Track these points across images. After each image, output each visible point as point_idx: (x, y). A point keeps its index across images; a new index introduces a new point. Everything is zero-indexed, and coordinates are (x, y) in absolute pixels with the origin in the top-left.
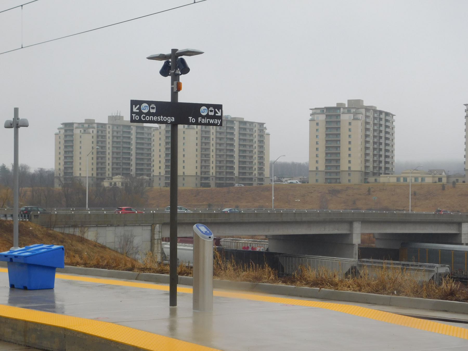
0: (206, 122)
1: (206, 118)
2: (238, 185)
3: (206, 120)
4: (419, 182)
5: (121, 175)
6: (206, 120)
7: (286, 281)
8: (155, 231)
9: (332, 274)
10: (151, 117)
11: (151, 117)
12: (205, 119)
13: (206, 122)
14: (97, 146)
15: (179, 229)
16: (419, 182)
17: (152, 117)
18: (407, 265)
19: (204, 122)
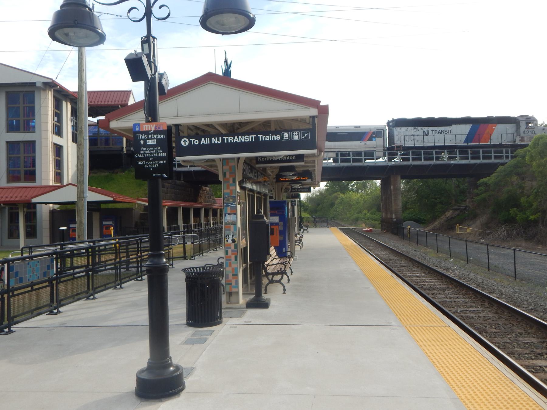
0: (270, 139)
1: (270, 135)
2: (290, 189)
3: (270, 136)
4: (273, 247)
5: (17, 211)
6: (270, 136)
7: (404, 196)
8: (500, 143)
9: (373, 220)
10: (163, 135)
11: (163, 135)
12: (156, 135)
13: (270, 139)
14: (530, 137)
15: (121, 254)
16: (273, 247)
17: (275, 136)
18: (405, 219)
19: (268, 139)
